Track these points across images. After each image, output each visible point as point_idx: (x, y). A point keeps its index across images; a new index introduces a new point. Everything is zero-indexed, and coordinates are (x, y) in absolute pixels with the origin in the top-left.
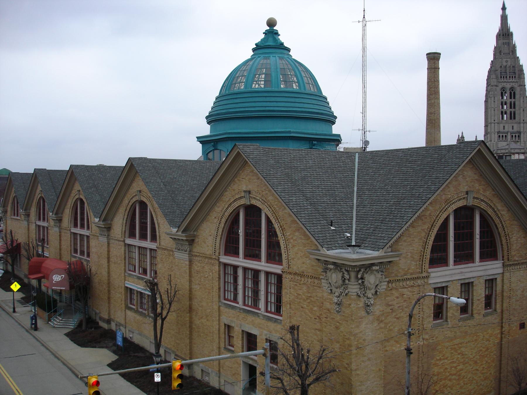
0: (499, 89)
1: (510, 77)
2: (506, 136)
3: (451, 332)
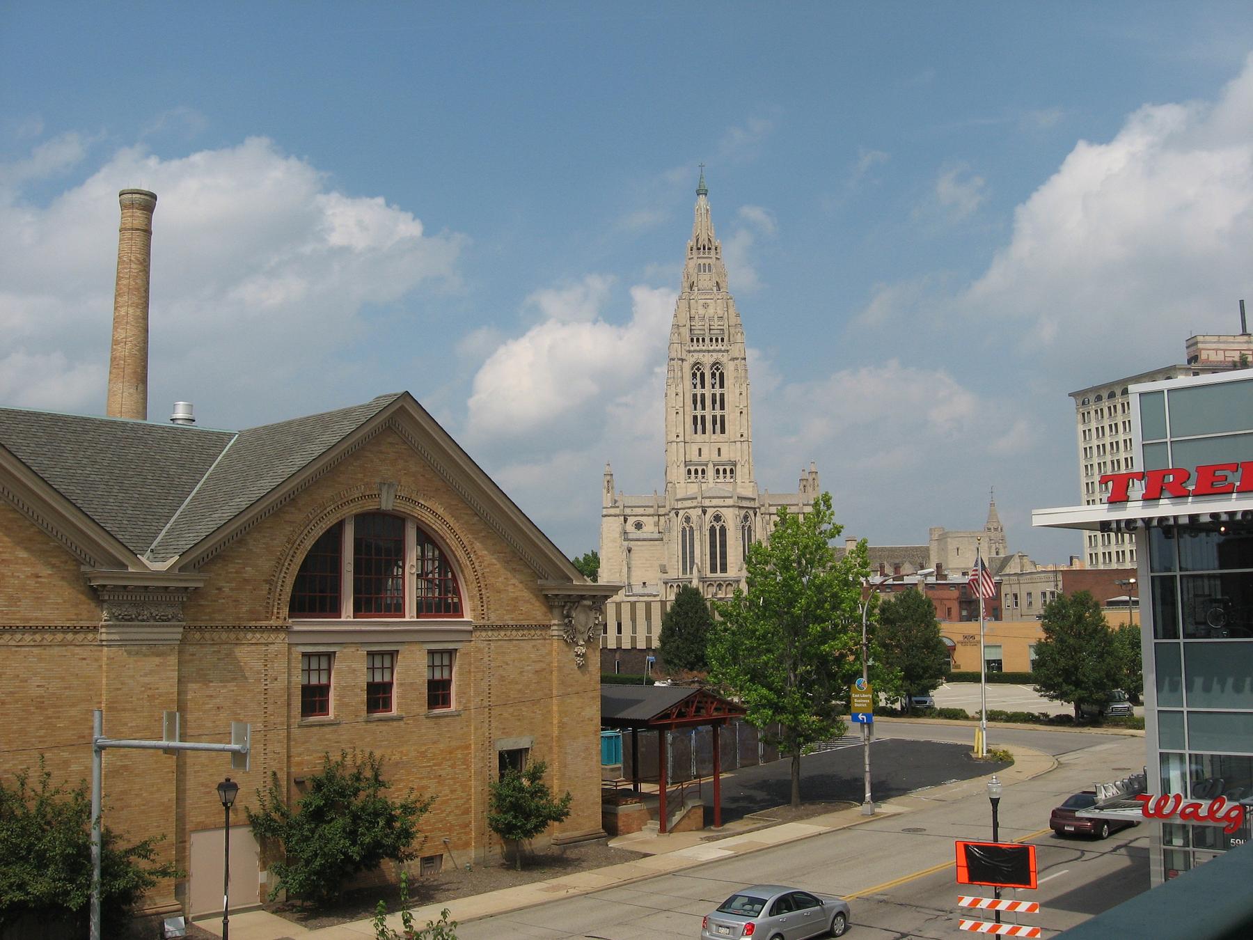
0: (687, 367)
1: (711, 340)
2: (703, 472)
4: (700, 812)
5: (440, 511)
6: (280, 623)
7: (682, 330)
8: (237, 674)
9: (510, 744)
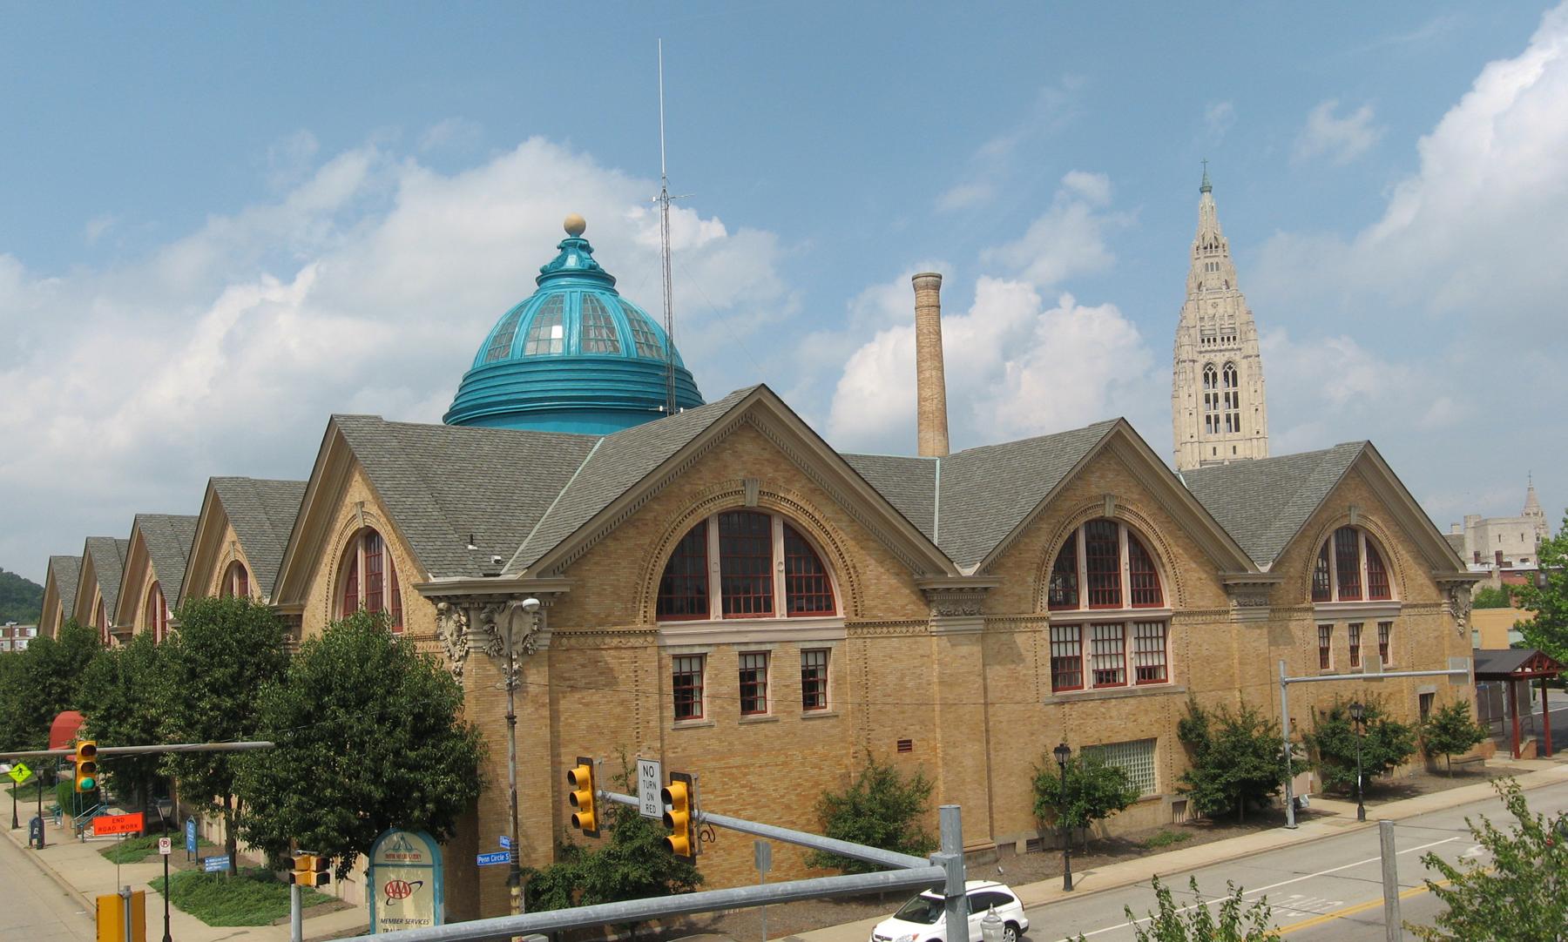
0: (1199, 368)
3: (721, 741)
4: (1534, 745)
5: (1144, 515)
6: (647, 627)
7: (1192, 331)
8: (609, 679)
9: (1424, 690)
